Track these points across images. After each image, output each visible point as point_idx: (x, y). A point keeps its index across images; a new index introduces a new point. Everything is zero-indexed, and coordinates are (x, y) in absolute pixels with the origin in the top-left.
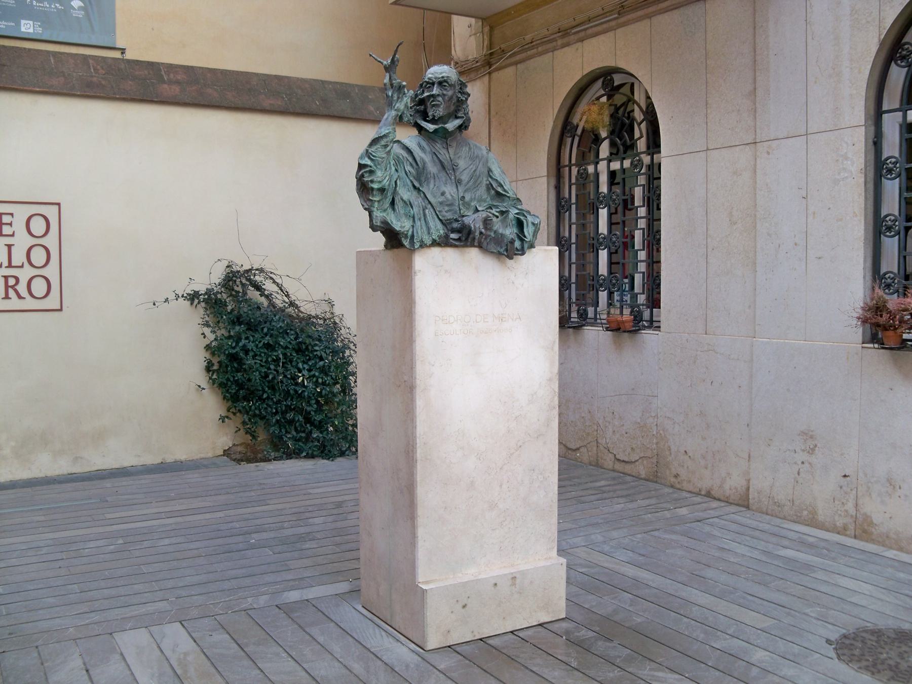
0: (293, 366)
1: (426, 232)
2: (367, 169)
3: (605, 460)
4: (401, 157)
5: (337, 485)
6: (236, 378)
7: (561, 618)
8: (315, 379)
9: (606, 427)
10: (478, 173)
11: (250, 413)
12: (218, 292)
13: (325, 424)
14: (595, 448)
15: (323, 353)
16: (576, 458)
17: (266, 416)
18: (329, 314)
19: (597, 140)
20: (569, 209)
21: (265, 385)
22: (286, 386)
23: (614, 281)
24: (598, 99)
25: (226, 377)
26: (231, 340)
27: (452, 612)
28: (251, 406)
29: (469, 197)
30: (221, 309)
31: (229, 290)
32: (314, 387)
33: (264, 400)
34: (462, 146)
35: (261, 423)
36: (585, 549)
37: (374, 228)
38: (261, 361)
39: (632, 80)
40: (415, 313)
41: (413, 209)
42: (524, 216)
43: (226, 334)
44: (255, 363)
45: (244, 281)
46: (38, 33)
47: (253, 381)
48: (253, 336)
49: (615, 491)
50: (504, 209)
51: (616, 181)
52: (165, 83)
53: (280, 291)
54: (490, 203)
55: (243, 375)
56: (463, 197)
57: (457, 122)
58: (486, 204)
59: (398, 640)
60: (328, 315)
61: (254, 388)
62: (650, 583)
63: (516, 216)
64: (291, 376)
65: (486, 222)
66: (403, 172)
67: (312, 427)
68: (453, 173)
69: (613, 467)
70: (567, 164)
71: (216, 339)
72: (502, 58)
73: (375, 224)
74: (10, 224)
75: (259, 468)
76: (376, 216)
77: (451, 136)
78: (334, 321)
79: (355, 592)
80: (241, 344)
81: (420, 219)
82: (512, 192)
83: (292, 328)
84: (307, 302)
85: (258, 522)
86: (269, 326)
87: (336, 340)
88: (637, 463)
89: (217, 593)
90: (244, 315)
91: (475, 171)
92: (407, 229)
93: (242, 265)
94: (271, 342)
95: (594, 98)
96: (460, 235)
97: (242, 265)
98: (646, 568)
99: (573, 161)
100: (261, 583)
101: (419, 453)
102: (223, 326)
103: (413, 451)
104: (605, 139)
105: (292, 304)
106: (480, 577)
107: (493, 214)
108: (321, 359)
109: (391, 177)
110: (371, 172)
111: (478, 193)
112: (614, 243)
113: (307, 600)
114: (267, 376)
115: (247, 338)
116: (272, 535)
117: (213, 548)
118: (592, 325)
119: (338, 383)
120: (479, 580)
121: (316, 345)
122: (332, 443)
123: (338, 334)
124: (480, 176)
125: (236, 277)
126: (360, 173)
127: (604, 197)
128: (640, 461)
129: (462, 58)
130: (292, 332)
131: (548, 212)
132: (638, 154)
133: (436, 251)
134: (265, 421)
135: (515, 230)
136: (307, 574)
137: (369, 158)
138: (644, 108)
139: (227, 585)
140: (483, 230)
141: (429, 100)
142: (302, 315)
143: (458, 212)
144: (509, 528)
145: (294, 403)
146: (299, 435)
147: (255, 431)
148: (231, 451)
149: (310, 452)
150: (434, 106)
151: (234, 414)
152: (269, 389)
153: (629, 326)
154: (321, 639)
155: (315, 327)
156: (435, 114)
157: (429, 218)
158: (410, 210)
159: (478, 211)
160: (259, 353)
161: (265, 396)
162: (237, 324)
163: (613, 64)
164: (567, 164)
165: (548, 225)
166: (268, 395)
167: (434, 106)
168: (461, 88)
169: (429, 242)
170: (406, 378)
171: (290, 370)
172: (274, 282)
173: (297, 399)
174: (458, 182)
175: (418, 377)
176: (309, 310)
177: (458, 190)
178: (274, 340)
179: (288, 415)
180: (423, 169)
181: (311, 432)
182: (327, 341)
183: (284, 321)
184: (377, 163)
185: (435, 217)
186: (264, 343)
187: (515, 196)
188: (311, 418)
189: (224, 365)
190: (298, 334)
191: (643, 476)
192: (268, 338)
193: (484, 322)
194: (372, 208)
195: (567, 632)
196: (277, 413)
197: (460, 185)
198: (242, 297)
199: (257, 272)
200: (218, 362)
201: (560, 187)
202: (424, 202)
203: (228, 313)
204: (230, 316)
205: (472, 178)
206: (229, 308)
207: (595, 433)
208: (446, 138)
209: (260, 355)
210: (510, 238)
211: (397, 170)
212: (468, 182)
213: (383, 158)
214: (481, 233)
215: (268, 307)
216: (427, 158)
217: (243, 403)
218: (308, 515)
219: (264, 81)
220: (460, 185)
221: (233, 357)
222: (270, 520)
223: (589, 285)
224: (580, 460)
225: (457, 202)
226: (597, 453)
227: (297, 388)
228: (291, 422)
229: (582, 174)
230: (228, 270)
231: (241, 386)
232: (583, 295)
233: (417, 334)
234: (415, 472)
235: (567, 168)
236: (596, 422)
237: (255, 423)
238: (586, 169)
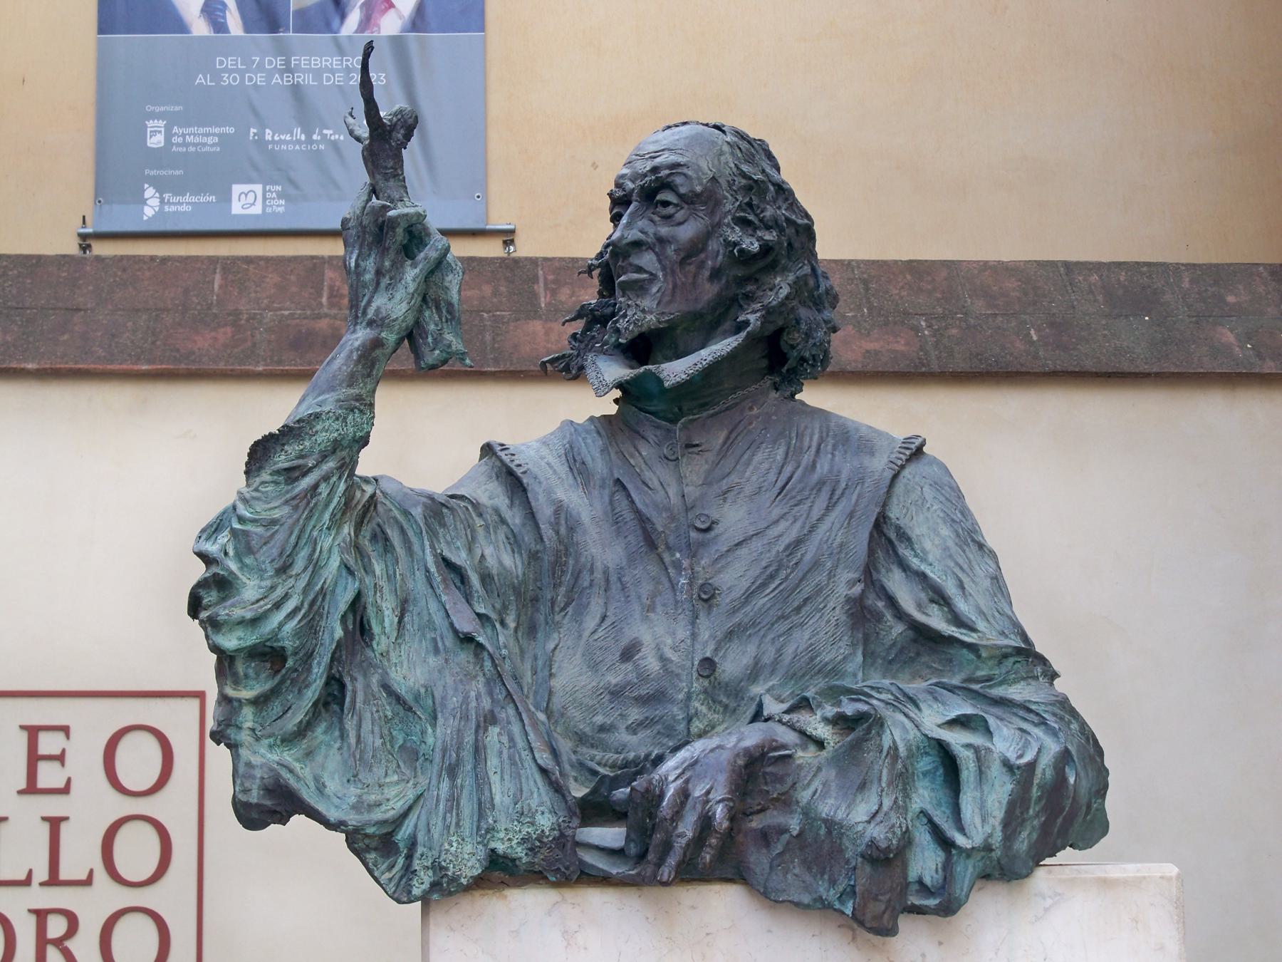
10: (809, 552)
29: (746, 660)
34: (753, 446)
46: (274, 213)
52: (540, 318)
56: (709, 665)
74: (60, 758)
91: (798, 542)
111: (801, 639)
124: (816, 564)
158: (423, 732)
169: (470, 866)
202: (491, 694)
205: (772, 577)
212: (749, 596)
213: (274, 522)
219: (866, 283)
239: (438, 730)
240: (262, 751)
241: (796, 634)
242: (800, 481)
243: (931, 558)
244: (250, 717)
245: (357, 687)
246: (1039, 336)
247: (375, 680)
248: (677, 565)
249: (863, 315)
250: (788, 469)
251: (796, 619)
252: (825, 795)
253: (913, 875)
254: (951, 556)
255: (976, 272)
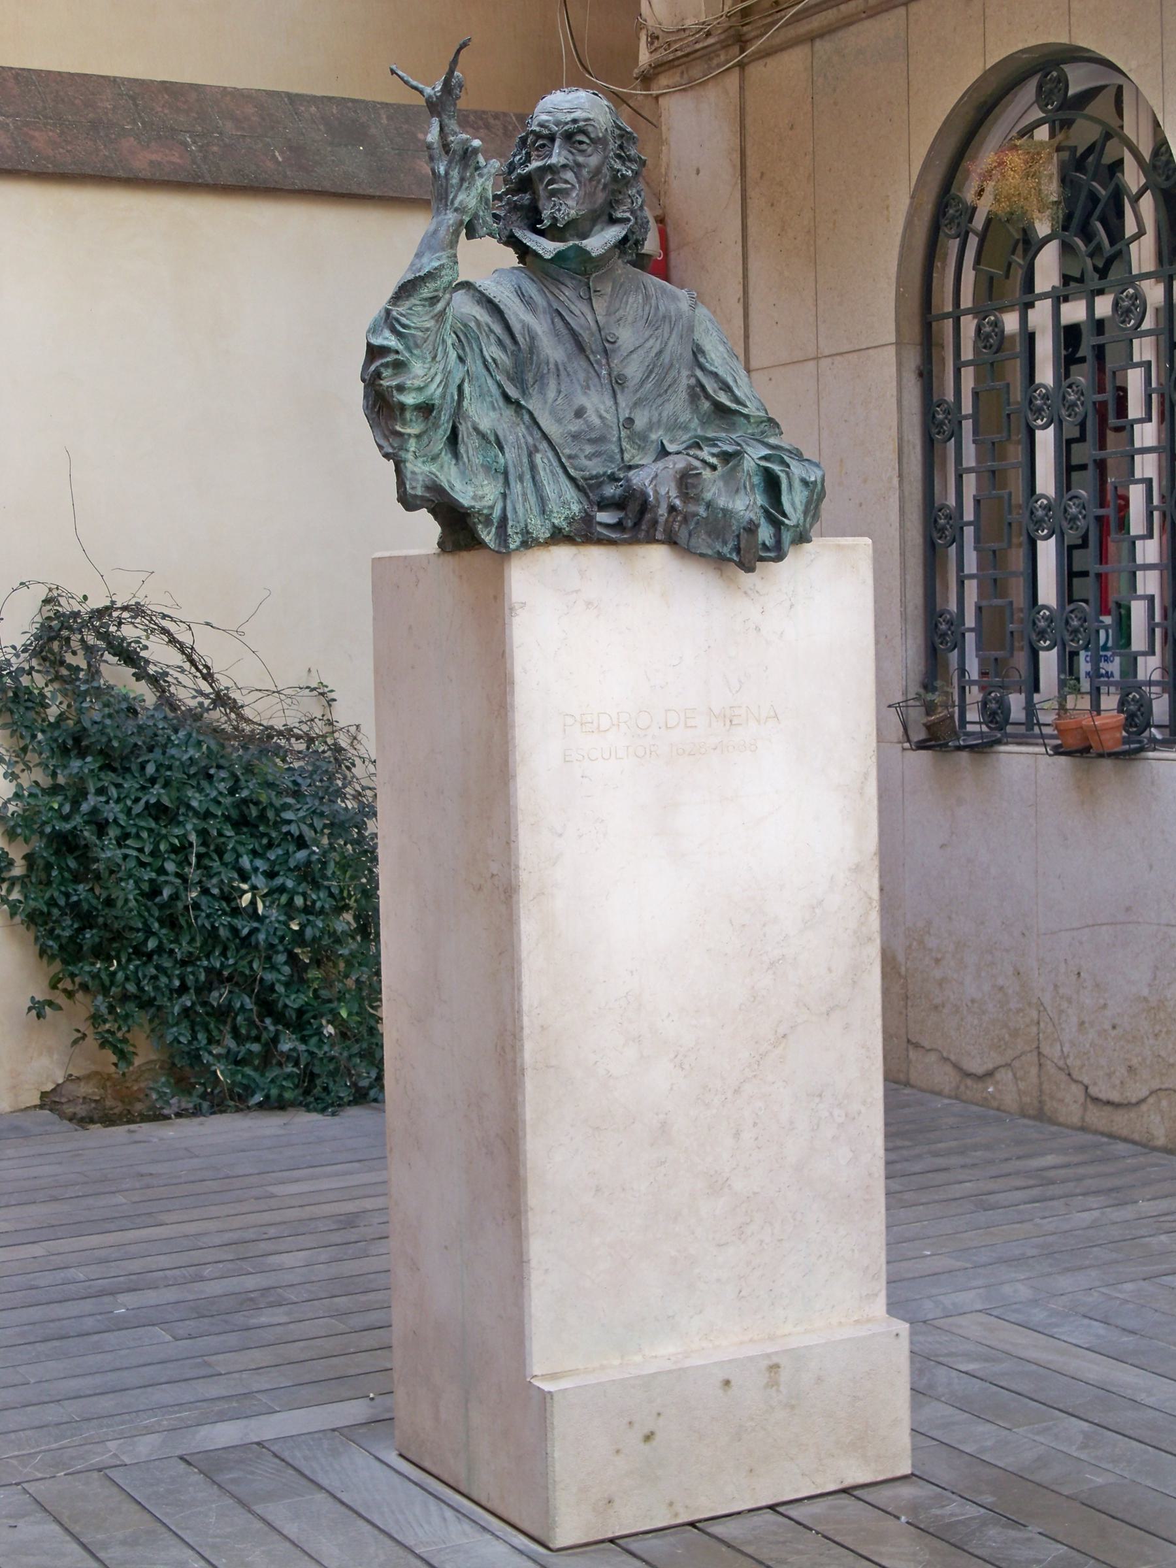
0: (225, 865)
1: (536, 510)
2: (388, 359)
3: (1062, 1101)
4: (472, 324)
5: (345, 1174)
6: (75, 898)
7: (899, 1473)
8: (284, 899)
9: (1061, 1012)
10: (666, 357)
11: (113, 989)
12: (20, 670)
13: (315, 1017)
14: (1034, 1071)
15: (305, 828)
16: (986, 1099)
17: (155, 999)
18: (320, 723)
19: (1030, 245)
20: (956, 433)
21: (151, 915)
22: (208, 916)
23: (1075, 623)
24: (1028, 131)
25: (47, 895)
26: (60, 798)
27: (618, 1451)
28: (114, 974)
29: (646, 420)
30: (32, 714)
31: (53, 663)
32: (282, 918)
33: (150, 956)
35: (142, 1017)
36: (983, 1318)
37: (408, 502)
38: (141, 850)
39: (1120, 80)
40: (512, 706)
41: (503, 454)
42: (783, 463)
43: (46, 782)
44: (125, 857)
45: (91, 639)
47: (120, 903)
48: (118, 786)
49: (1079, 1179)
50: (730, 448)
51: (1080, 354)
53: (187, 666)
54: (700, 432)
55: (92, 890)
56: (630, 421)
57: (613, 233)
58: (685, 437)
59: (484, 1529)
60: (319, 728)
61: (123, 924)
62: (1142, 1397)
63: (764, 463)
64: (221, 890)
65: (686, 481)
66: (479, 363)
67: (280, 1027)
68: (604, 361)
69: (1083, 1120)
70: (951, 309)
71: (17, 796)
72: (774, 23)
73: (409, 491)
75: (137, 1137)
76: (413, 473)
77: (597, 268)
78: (335, 744)
79: (382, 1422)
80: (85, 807)
81: (521, 478)
82: (756, 404)
83: (222, 762)
84: (260, 694)
85: (136, 1265)
86: (160, 758)
87: (340, 794)
88: (1144, 1107)
89: (28, 1433)
90: (94, 730)
91: (660, 352)
92: (490, 503)
93: (85, 598)
94: (166, 801)
95: (1014, 133)
96: (622, 515)
97: (85, 598)
98: (1137, 1362)
99: (967, 301)
100: (142, 1407)
101: (530, 1052)
102: (38, 761)
103: (513, 1047)
104: (1047, 240)
105: (221, 699)
106: (687, 1363)
107: (704, 461)
108: (301, 843)
109: (447, 374)
110: (399, 366)
111: (669, 409)
112: (1074, 519)
113: (258, 1444)
114: (155, 891)
115: (101, 791)
116: (171, 1295)
117: (17, 1329)
118: (1021, 740)
119: (346, 908)
120: (684, 1370)
121: (285, 807)
122: (332, 1067)
123: (345, 778)
124: (671, 365)
125: (70, 628)
126: (373, 368)
127: (1046, 397)
128: (1151, 1100)
129: (668, 26)
130: (223, 774)
131: (900, 439)
132: (1132, 280)
133: (562, 554)
134: (152, 1010)
135: (760, 500)
136: (260, 1383)
137: (394, 331)
138: (1147, 155)
139: (51, 1414)
140: (678, 502)
141: (541, 180)
142: (247, 728)
143: (618, 457)
144: (762, 1241)
145: (231, 961)
146: (243, 1050)
147: (125, 1040)
148: (62, 1096)
149: (274, 1092)
150: (554, 193)
151: (70, 994)
152: (162, 924)
153: (1113, 740)
154: (291, 1530)
155: (284, 761)
156: (557, 215)
157: (543, 475)
158: (496, 456)
159: (667, 454)
160: (134, 831)
161: (152, 944)
162: (73, 754)
163: (1064, 39)
164: (951, 309)
165: (900, 476)
166: (161, 942)
167: (554, 193)
168: (621, 147)
169: (543, 534)
170: (494, 868)
171: (219, 873)
172: (173, 641)
173: (238, 951)
174: (617, 383)
175: (522, 864)
176: (268, 714)
177: (616, 403)
178: (174, 794)
179: (215, 994)
180: (531, 352)
181: (275, 1040)
182: (315, 796)
183: (199, 744)
184: (411, 344)
185: (559, 471)
186: (147, 802)
187: (762, 414)
188: (275, 1002)
189: (41, 863)
190: (237, 780)
191: (1161, 1141)
192: (157, 789)
193: (687, 727)
194: (402, 454)
195: (914, 1507)
196: (183, 989)
197: (623, 390)
198: (86, 682)
199: (126, 615)
200: (25, 857)
201: (930, 372)
202: (531, 435)
203: (50, 724)
204: (56, 734)
205: (651, 372)
206: (53, 712)
207: (1034, 1029)
208: (586, 274)
209: (138, 836)
210: (747, 518)
211: (461, 359)
212: (642, 382)
213: (427, 329)
214: (672, 509)
215: (157, 707)
216: (540, 326)
217: (93, 964)
218: (264, 1246)
220: (623, 390)
221: (65, 843)
222: (164, 1261)
223: (1012, 633)
224: (995, 1104)
225: (615, 433)
226: (1041, 1084)
227: (238, 923)
228: (223, 1014)
229: (988, 336)
230: (48, 611)
231: (86, 919)
232: (996, 660)
233: (518, 758)
234: (520, 1098)
235: (949, 323)
236: (1034, 1000)
237: (127, 1017)
238: (997, 324)
239: (507, 455)
240: (420, 465)
241: (666, 405)
242: (655, 315)
243: (716, 364)
244: (414, 445)
245: (463, 429)
246: (283, 158)
247: (469, 424)
248: (598, 362)
249: (138, 129)
250: (647, 308)
251: (665, 397)
252: (719, 496)
253: (760, 541)
254: (727, 363)
255: (219, 96)
